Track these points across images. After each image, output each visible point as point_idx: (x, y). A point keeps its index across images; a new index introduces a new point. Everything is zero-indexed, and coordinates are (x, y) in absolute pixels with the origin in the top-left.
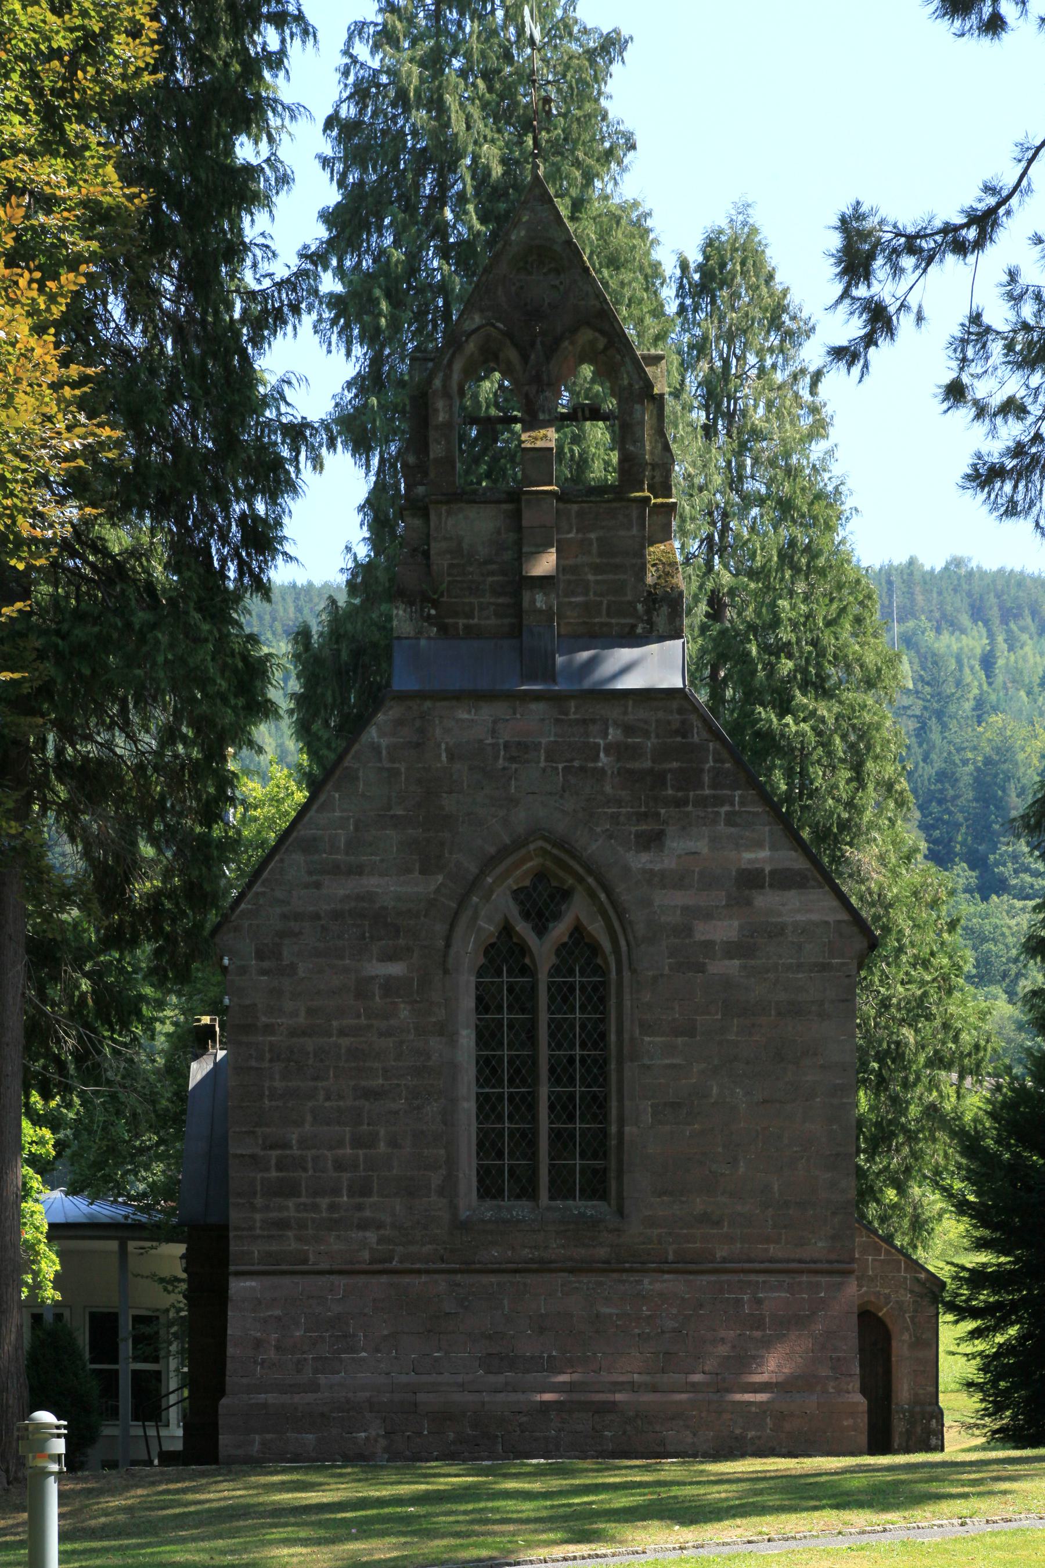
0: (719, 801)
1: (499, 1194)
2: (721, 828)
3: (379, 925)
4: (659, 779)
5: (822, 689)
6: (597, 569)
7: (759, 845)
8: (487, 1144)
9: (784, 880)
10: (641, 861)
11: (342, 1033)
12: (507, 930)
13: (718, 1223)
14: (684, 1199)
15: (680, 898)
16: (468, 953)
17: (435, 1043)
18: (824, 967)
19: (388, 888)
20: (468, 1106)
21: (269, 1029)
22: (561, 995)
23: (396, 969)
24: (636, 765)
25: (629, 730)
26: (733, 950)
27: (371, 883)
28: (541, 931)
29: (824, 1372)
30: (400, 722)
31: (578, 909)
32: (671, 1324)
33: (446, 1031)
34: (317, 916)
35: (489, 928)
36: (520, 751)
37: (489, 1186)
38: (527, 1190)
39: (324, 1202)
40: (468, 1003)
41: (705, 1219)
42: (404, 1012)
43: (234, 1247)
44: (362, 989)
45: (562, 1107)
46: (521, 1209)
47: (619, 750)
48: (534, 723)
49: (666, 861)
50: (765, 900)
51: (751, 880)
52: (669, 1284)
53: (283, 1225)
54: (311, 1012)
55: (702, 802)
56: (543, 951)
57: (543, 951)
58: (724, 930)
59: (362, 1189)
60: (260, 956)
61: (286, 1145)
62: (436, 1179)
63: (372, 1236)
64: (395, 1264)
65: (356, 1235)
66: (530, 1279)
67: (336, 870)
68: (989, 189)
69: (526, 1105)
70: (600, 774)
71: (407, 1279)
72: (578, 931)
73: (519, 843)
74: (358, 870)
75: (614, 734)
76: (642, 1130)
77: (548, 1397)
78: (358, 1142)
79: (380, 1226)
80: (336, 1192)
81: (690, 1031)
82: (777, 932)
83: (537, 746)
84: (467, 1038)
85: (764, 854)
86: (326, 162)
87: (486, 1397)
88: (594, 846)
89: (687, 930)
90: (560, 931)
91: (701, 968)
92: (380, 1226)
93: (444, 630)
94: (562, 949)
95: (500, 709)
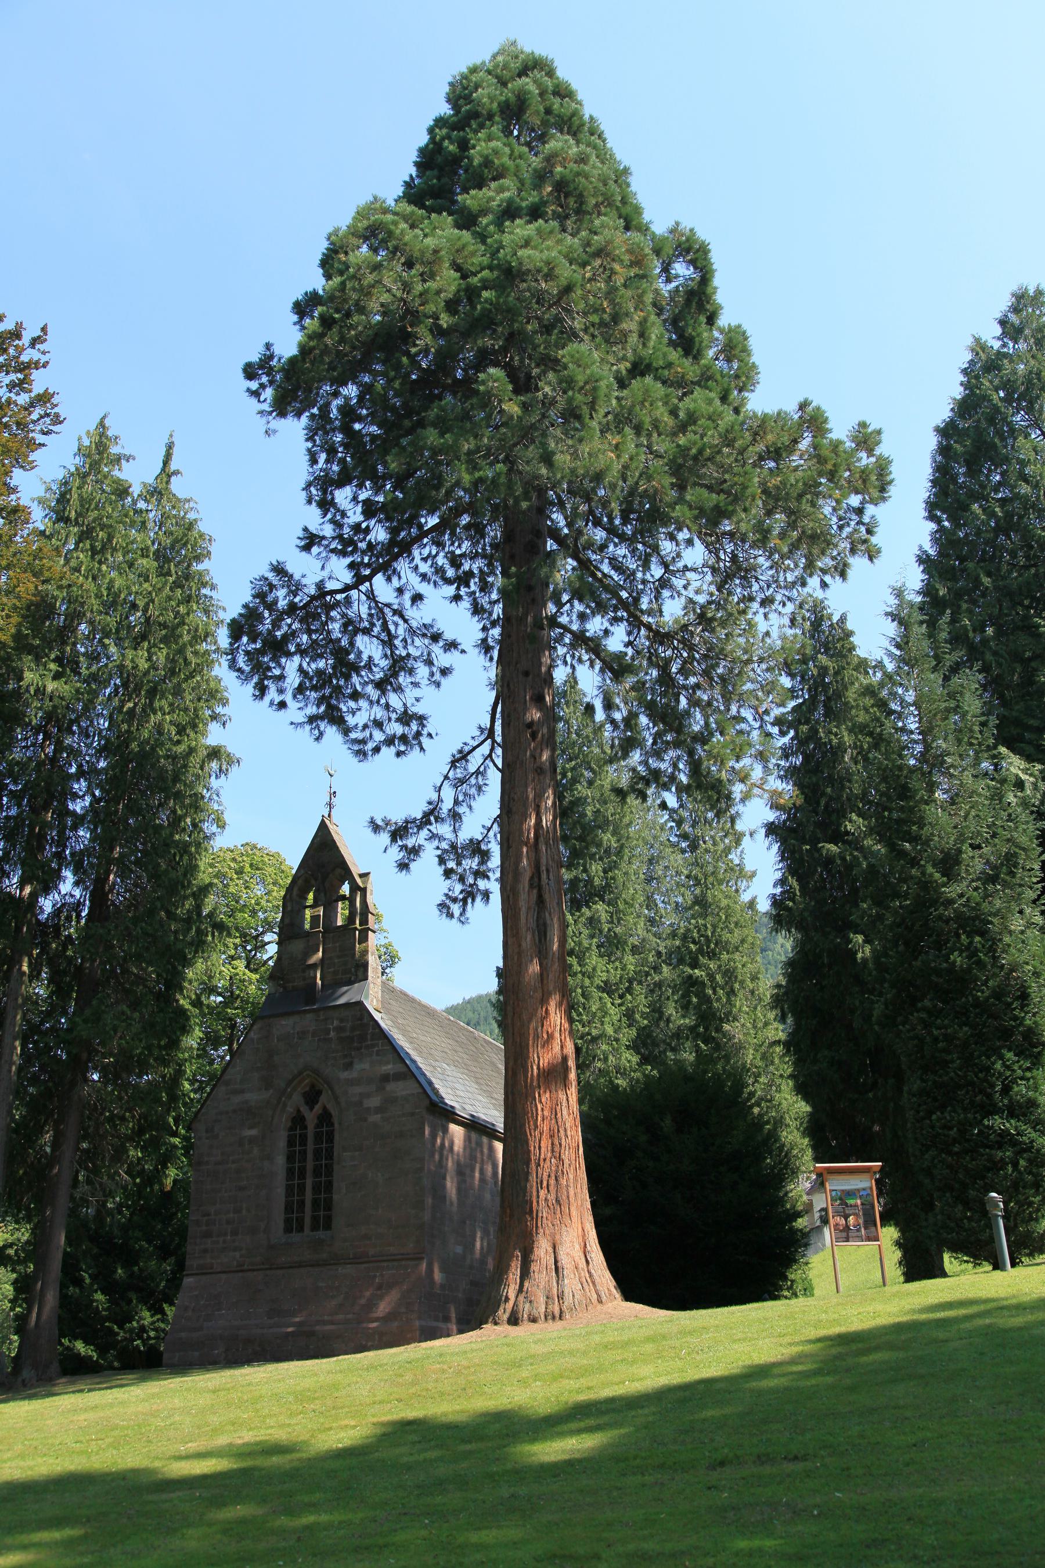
0: (373, 1046)
1: (291, 1231)
5: (712, 955)
7: (388, 1063)
10: (345, 1075)
11: (233, 1162)
15: (357, 1090)
16: (283, 1122)
19: (253, 1097)
20: (280, 1191)
22: (318, 1137)
23: (253, 1132)
24: (343, 1035)
25: (341, 1020)
26: (379, 1110)
27: (248, 1096)
29: (403, 1310)
31: (323, 1099)
36: (302, 1035)
37: (288, 1230)
39: (221, 1239)
40: (282, 1144)
42: (256, 1151)
43: (187, 1263)
45: (316, 1188)
46: (295, 1237)
47: (339, 1029)
48: (308, 1022)
50: (391, 1087)
51: (386, 1078)
53: (205, 1251)
56: (311, 1118)
57: (311, 1118)
58: (374, 1102)
61: (209, 1215)
63: (237, 1254)
68: (430, 803)
69: (302, 1188)
72: (325, 1109)
73: (300, 1073)
74: (242, 1091)
75: (336, 1023)
76: (342, 1196)
77: (290, 1329)
84: (281, 1160)
85: (390, 1066)
90: (318, 1108)
91: (365, 1120)
93: (285, 988)
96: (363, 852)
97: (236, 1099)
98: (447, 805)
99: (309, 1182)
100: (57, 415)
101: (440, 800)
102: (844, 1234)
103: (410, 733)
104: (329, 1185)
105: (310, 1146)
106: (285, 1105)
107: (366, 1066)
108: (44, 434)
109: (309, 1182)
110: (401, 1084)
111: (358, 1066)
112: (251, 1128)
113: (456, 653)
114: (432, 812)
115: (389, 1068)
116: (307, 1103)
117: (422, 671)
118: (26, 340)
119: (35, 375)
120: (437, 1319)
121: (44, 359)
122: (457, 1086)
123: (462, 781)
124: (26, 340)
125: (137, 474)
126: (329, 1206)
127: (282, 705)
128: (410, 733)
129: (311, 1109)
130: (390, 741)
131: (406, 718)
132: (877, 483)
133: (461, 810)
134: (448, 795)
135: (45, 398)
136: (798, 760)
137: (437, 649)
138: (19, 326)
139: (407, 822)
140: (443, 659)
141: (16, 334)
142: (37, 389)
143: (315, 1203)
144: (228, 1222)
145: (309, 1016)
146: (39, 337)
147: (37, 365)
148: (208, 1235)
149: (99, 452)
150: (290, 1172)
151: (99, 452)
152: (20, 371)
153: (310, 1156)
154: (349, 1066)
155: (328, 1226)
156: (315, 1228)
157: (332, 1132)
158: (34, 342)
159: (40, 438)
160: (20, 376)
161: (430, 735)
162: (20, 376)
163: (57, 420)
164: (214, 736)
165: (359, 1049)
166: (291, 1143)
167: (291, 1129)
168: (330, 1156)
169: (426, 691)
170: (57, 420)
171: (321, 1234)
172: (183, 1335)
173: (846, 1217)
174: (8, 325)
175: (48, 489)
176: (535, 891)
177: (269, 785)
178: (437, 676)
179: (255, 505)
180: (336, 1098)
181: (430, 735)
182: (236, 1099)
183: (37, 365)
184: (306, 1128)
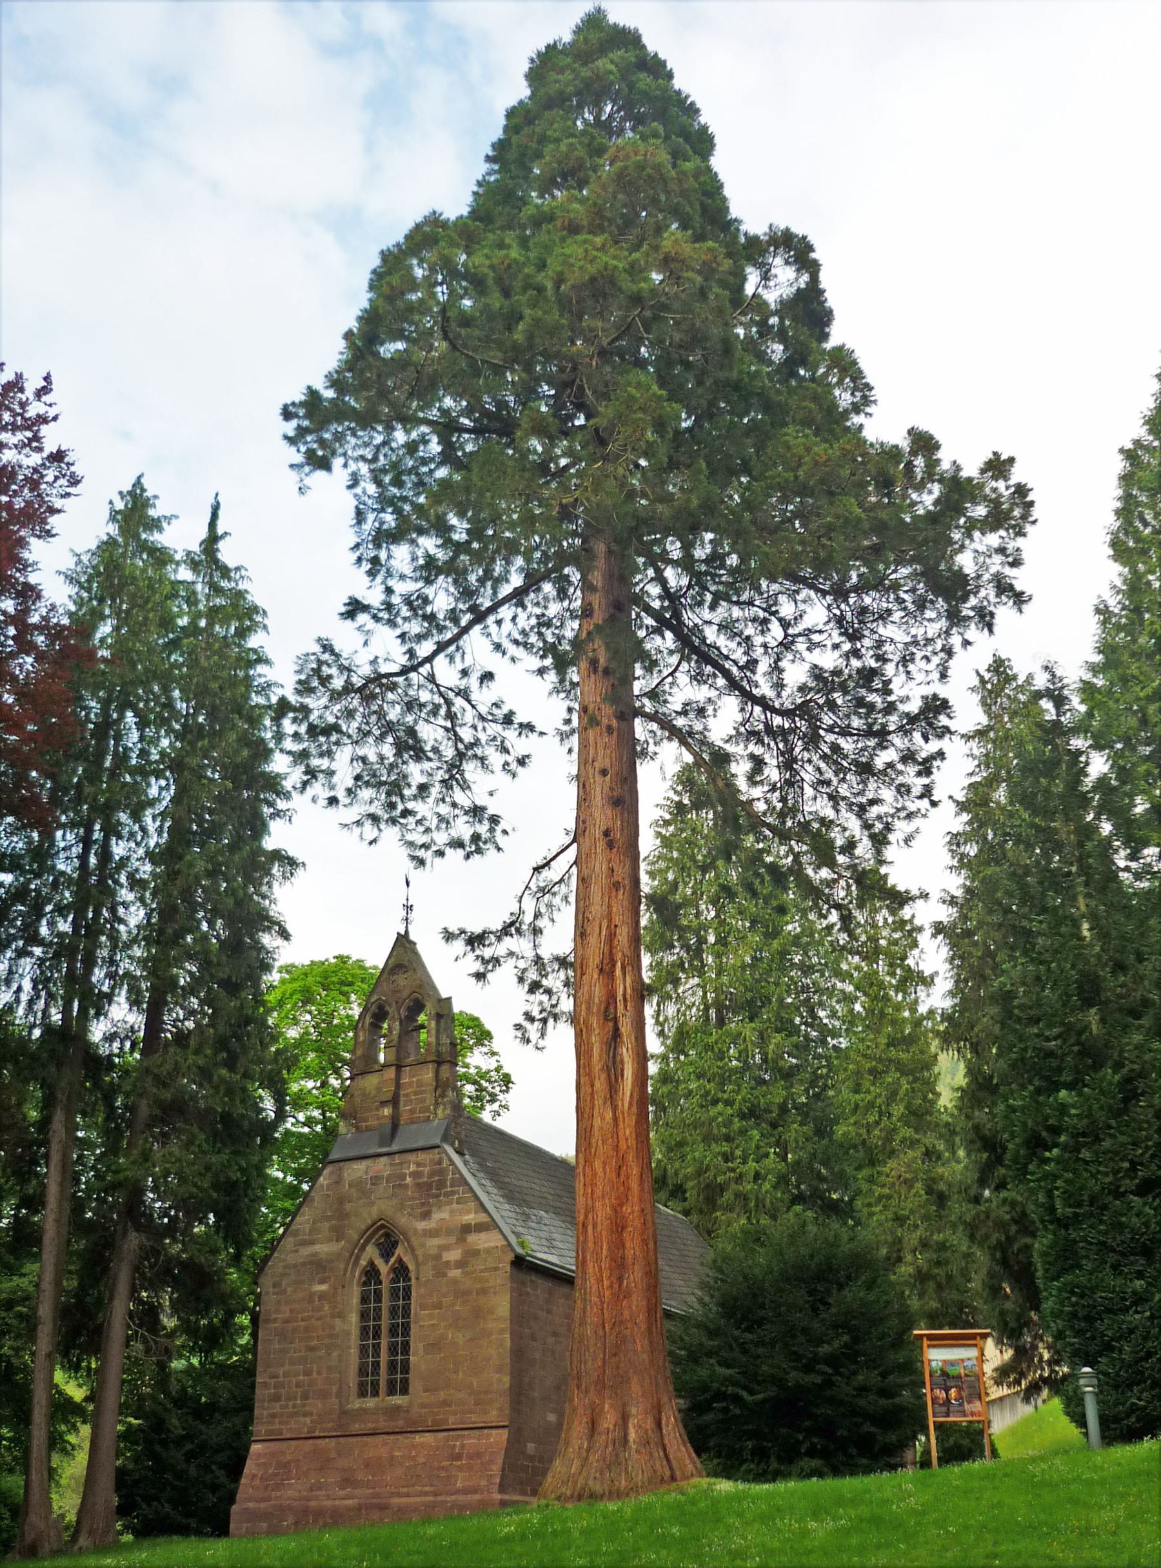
0: (453, 1193)
2: (455, 1206)
3: (319, 1267)
4: (429, 1186)
6: (416, 1093)
7: (469, 1212)
8: (362, 1371)
9: (480, 1228)
10: (421, 1225)
12: (371, 1263)
13: (449, 1405)
14: (1118, 1469)
15: (436, 1242)
17: (338, 1322)
18: (496, 1269)
19: (324, 1249)
20: (354, 1352)
21: (275, 1320)
22: (394, 1293)
25: (418, 1165)
26: (461, 1264)
27: (317, 1248)
28: (371, 1263)
30: (331, 1173)
31: (399, 1251)
32: (421, 1460)
33: (341, 1315)
34: (295, 1266)
35: (363, 1263)
36: (376, 1180)
38: (375, 1393)
40: (355, 1300)
41: (446, 1403)
44: (310, 1298)
45: (393, 1350)
46: (370, 1403)
47: (415, 1175)
49: (430, 1224)
50: (472, 1238)
51: (466, 1229)
52: (428, 1438)
53: (274, 1416)
54: (291, 1311)
55: (447, 1194)
56: (384, 1268)
58: (454, 1255)
59: (305, 1397)
60: (274, 1286)
62: (334, 1389)
63: (308, 1420)
64: (317, 1434)
65: (302, 1419)
66: (369, 1439)
67: (304, 1243)
70: (406, 1187)
71: (320, 1441)
74: (312, 1243)
75: (413, 1168)
78: (308, 1373)
79: (311, 1415)
80: (295, 1398)
81: (439, 1306)
82: (476, 1253)
83: (382, 1177)
84: (354, 1318)
85: (472, 1216)
86: (1103, 611)
87: (337, 1503)
88: (403, 1220)
89: (438, 1257)
90: (393, 1260)
91: (445, 1275)
92: (311, 1415)
93: (357, 1128)
94: (394, 1270)
95: (369, 1162)
96: (448, 973)
97: (305, 1251)
98: (528, 918)
99: (384, 1342)
100: (73, 475)
101: (521, 912)
102: (944, 1409)
103: (482, 835)
104: (406, 1347)
105: (385, 1304)
106: (358, 1258)
107: (445, 1215)
108: (62, 496)
109: (384, 1342)
110: (483, 1236)
111: (437, 1216)
112: (322, 1282)
113: (533, 737)
114: (512, 924)
115: (471, 1218)
116: (382, 1256)
117: (496, 759)
118: (29, 393)
119: (44, 430)
120: (524, 1493)
121: (52, 413)
122: (555, 1236)
123: (544, 891)
124: (29, 393)
125: (181, 536)
126: (406, 1369)
127: (333, 801)
128: (482, 835)
129: (387, 1262)
130: (457, 844)
131: (476, 812)
132: (1013, 513)
133: (540, 923)
134: (529, 905)
135: (58, 457)
136: (972, 850)
137: (511, 735)
138: (19, 376)
139: (484, 932)
140: (519, 745)
141: (16, 385)
142: (50, 447)
143: (392, 1366)
144: (298, 1385)
145: (383, 1160)
146: (44, 388)
147: (43, 420)
148: (276, 1398)
149: (135, 513)
150: (364, 1332)
151: (135, 513)
152: (29, 428)
153: (385, 1314)
154: (426, 1215)
155: (405, 1391)
156: (391, 1391)
157: (409, 1287)
158: (41, 393)
159: (58, 503)
160: (29, 434)
161: (505, 832)
162: (29, 434)
163: (75, 481)
164: (277, 837)
165: (438, 1196)
166: (364, 1300)
167: (365, 1284)
168: (407, 1312)
169: (500, 779)
170: (75, 481)
171: (398, 1400)
172: (251, 1505)
173: (947, 1391)
174: (7, 376)
175: (79, 562)
176: (611, 1024)
177: (337, 892)
178: (514, 766)
179: (305, 565)
180: (413, 1250)
181: (505, 832)
182: (305, 1251)
183: (43, 420)
184: (381, 1283)
